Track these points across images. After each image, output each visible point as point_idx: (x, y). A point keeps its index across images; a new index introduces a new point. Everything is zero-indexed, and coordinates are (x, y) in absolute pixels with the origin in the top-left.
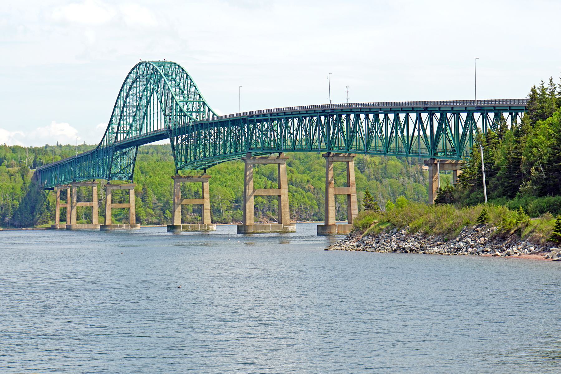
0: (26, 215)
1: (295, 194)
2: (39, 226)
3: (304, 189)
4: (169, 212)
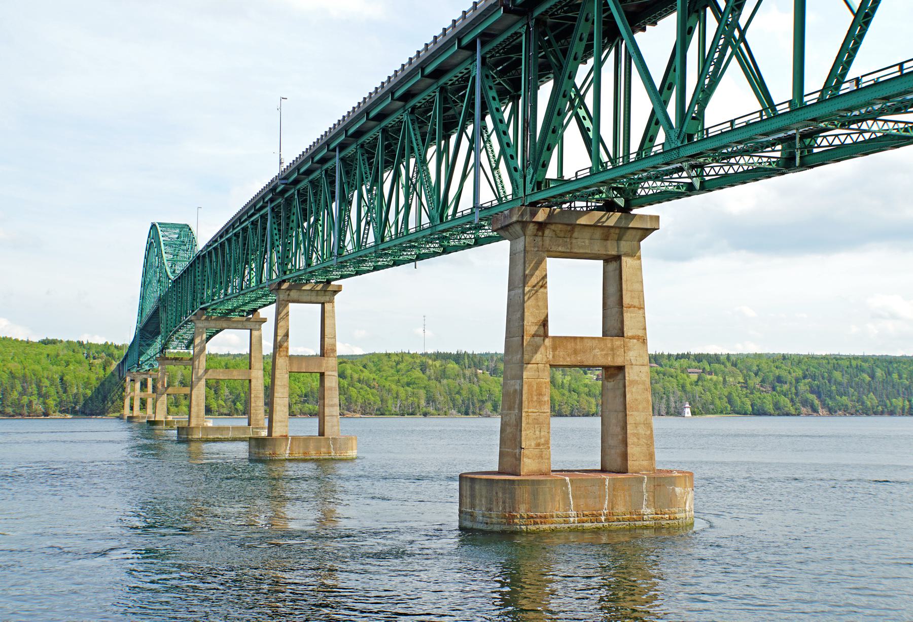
2: (111, 415)
3: (369, 386)
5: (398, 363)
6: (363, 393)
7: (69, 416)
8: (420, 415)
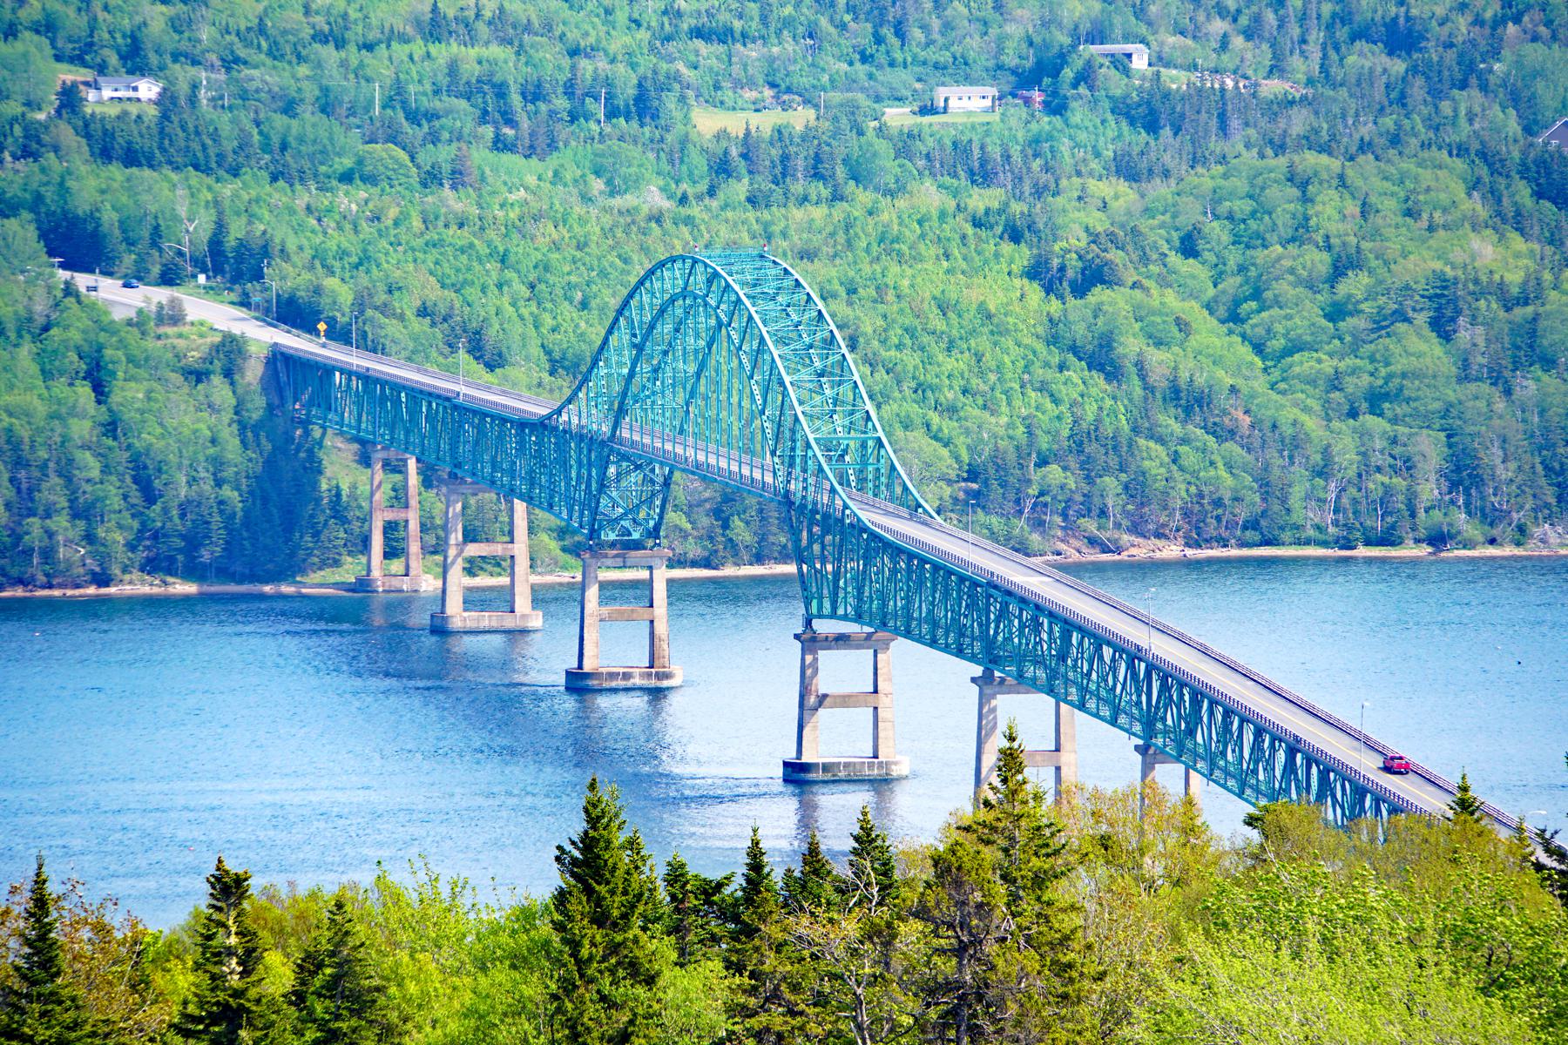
0: (269, 541)
1: (1183, 449)
4: (742, 524)
5: (1339, 270)
6: (1189, 456)
7: (604, 670)
8: (1418, 541)
